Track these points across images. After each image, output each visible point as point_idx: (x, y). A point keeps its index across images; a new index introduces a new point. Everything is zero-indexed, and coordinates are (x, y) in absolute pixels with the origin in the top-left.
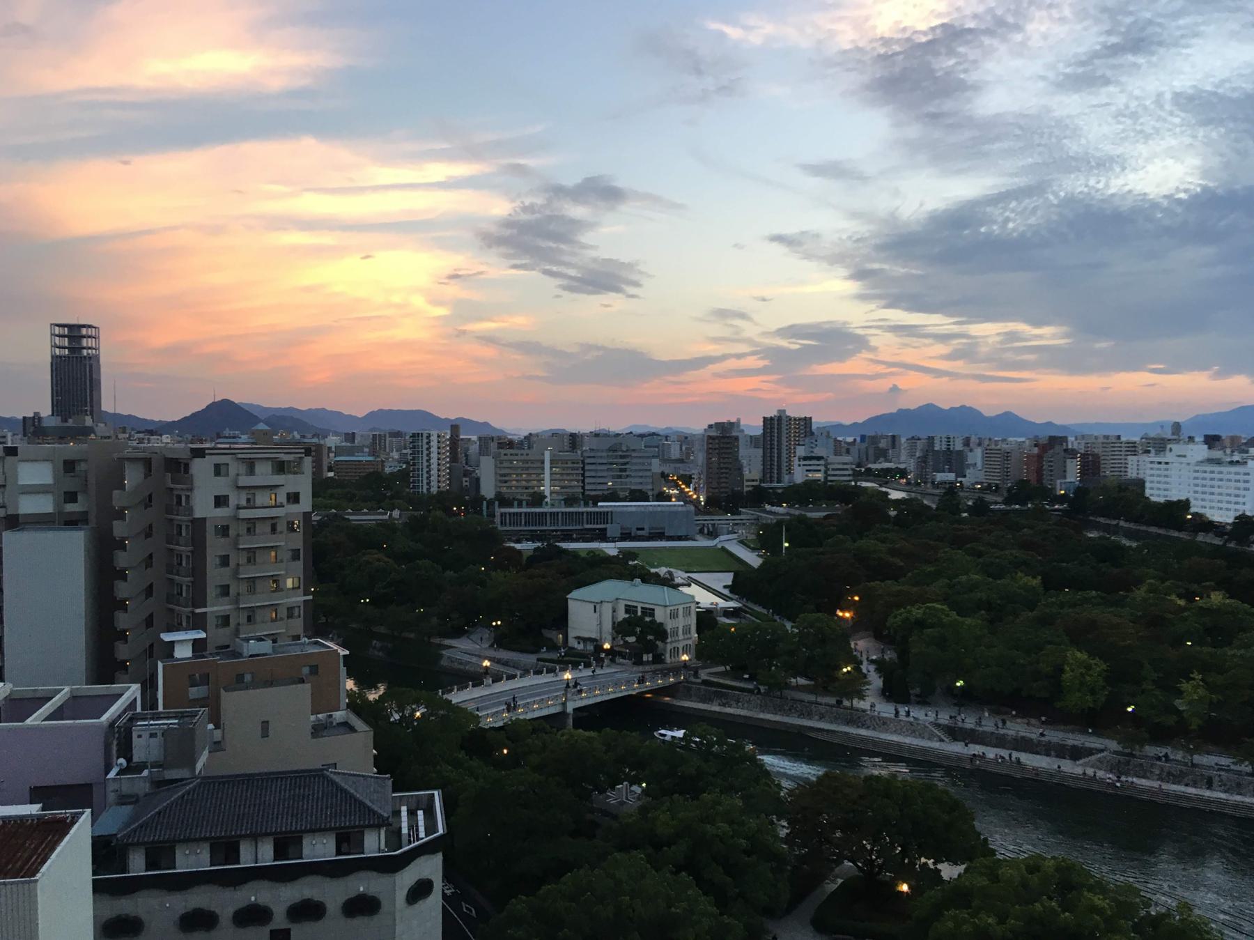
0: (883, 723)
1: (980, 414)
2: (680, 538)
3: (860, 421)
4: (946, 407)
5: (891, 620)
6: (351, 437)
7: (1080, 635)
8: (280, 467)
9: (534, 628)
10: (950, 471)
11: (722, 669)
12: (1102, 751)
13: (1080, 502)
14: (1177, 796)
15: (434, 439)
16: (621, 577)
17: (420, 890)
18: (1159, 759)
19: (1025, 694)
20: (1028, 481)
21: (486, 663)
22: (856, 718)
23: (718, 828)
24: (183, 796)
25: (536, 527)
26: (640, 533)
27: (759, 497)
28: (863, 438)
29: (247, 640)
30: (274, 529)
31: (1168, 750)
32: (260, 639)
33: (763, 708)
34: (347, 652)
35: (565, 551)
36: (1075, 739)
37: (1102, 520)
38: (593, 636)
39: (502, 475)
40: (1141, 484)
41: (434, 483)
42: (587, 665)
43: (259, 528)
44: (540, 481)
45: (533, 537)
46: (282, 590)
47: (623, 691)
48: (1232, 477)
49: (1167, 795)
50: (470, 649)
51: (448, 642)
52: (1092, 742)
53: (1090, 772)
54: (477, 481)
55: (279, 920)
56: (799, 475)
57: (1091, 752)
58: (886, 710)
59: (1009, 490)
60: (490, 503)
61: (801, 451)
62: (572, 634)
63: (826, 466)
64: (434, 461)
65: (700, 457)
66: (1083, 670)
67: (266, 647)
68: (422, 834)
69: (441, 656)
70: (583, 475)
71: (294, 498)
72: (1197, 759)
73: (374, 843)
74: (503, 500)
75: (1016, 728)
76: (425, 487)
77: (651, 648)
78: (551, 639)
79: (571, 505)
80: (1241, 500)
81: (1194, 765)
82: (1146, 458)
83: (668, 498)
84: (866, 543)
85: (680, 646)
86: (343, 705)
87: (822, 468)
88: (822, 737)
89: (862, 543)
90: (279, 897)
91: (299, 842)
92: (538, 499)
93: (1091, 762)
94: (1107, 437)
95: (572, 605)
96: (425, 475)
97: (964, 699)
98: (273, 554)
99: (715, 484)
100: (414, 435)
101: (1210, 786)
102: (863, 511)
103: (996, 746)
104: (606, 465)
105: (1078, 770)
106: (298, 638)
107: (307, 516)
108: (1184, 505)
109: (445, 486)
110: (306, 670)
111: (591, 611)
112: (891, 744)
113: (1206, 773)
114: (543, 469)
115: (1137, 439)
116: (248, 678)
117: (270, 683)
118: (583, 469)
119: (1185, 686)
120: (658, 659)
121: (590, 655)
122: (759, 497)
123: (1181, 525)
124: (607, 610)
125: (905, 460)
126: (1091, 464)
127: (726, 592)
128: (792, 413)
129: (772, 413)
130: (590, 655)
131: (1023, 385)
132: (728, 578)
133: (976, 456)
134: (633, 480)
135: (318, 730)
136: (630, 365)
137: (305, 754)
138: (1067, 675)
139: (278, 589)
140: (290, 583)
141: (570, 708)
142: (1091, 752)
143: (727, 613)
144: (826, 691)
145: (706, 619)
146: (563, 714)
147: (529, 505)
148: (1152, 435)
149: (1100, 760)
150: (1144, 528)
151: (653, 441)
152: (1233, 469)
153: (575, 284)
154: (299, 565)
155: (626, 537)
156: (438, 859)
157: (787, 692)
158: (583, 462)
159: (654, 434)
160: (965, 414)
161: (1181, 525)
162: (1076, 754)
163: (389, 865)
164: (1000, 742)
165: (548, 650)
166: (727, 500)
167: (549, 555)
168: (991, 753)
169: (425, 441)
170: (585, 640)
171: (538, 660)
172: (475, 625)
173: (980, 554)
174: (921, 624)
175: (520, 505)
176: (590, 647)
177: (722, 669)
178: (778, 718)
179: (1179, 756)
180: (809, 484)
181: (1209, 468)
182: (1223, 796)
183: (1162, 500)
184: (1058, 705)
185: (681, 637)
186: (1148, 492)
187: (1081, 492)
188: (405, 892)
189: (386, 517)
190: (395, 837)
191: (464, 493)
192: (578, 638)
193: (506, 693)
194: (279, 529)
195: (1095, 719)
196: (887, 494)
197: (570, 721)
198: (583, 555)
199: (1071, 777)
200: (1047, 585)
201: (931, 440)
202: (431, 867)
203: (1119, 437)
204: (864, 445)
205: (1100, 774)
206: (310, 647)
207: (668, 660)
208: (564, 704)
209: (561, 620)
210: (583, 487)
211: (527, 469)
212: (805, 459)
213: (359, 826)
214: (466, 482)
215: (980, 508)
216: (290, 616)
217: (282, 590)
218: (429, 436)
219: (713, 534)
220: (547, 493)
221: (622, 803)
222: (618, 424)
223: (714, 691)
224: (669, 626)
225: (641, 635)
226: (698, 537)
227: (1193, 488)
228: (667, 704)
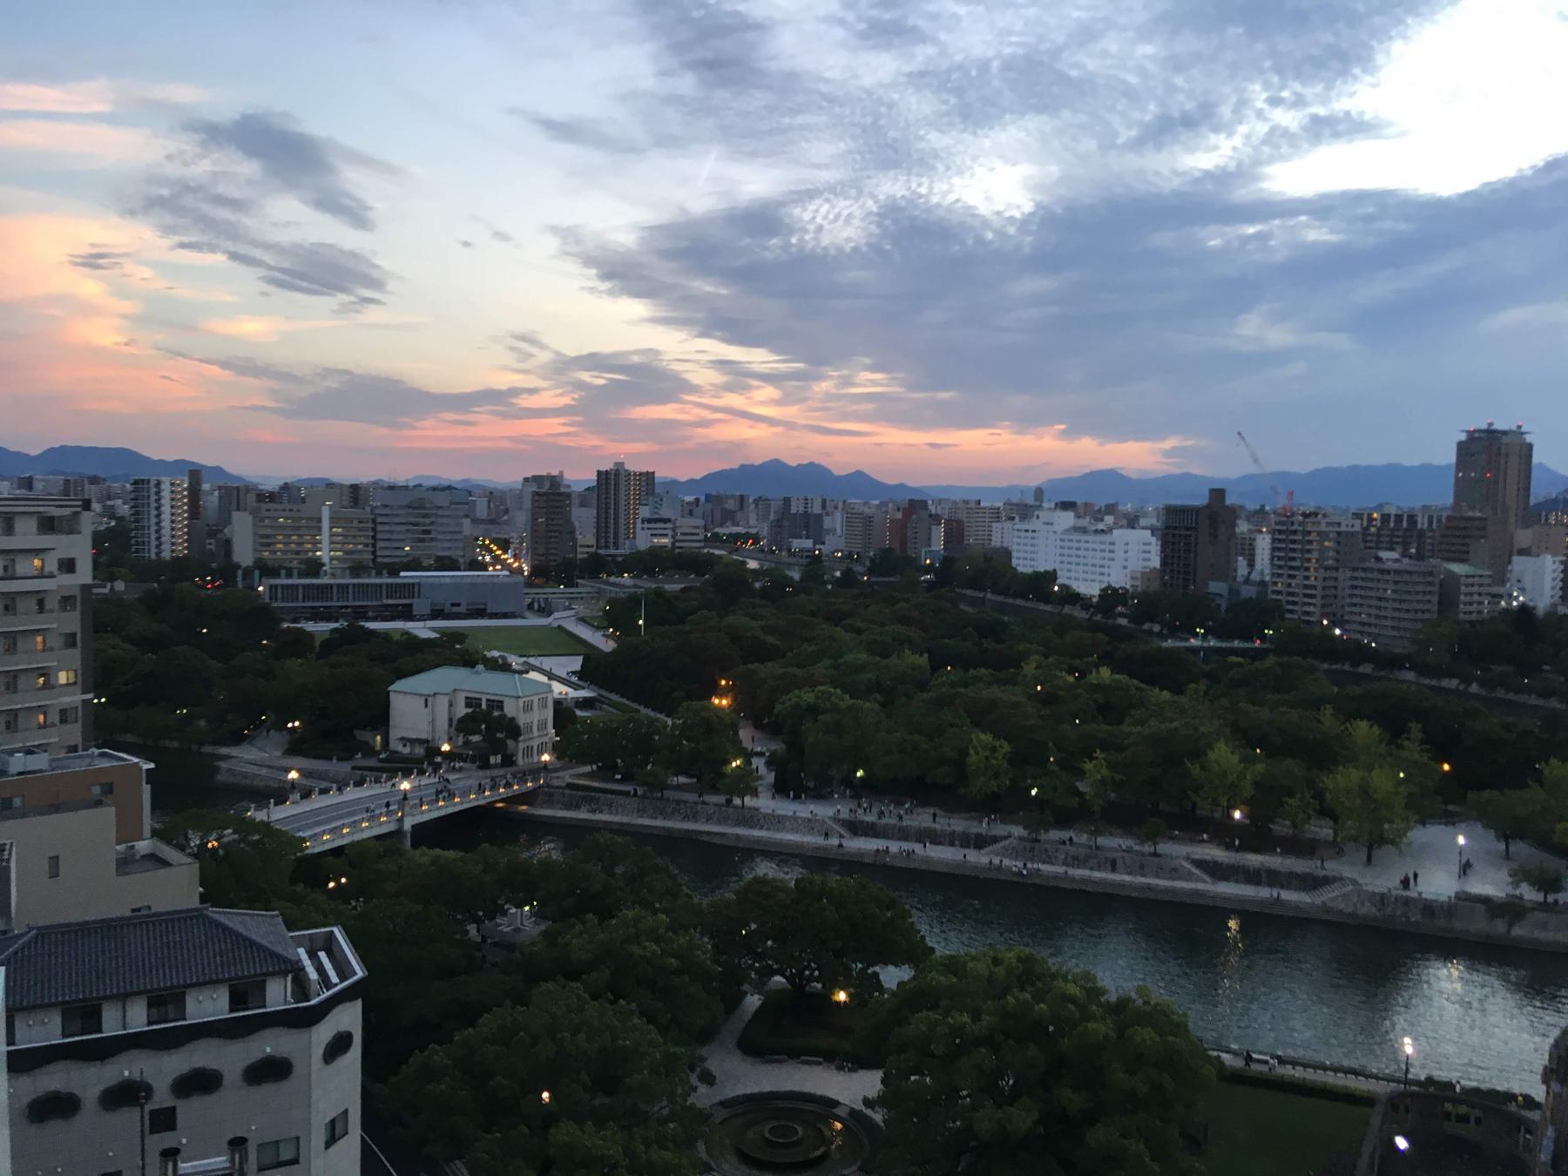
0: (777, 822)
1: (785, 465)
2: (505, 616)
3: (698, 477)
4: (794, 464)
5: (778, 707)
6: (28, 483)
7: (981, 716)
8: (48, 525)
9: (345, 726)
10: (808, 537)
11: (587, 769)
12: (1006, 838)
13: (947, 571)
14: (1084, 881)
15: (166, 487)
16: (452, 662)
17: (339, 1045)
18: (1064, 843)
19: (928, 784)
20: (890, 550)
21: (293, 775)
22: (750, 818)
23: (645, 948)
24: (16, 953)
25: (320, 602)
26: (455, 609)
27: (596, 566)
28: (708, 498)
29: (11, 753)
30: (41, 603)
31: (1071, 833)
32: (29, 751)
33: (641, 812)
34: (152, 766)
35: (373, 632)
36: (982, 828)
37: (968, 592)
38: (424, 736)
39: (262, 537)
40: (1007, 553)
41: (166, 547)
42: (421, 772)
43: (21, 605)
44: (316, 544)
45: (327, 616)
46: (53, 687)
47: (473, 800)
48: (1099, 547)
49: (1073, 879)
50: (250, 759)
51: (224, 751)
52: (999, 829)
53: (996, 861)
54: (228, 544)
55: (162, 1097)
56: (644, 540)
57: (995, 840)
58: (785, 807)
59: (872, 560)
60: (248, 573)
61: (645, 512)
62: (395, 734)
63: (674, 529)
64: (166, 517)
65: (521, 518)
66: (987, 753)
67: (40, 762)
68: (335, 979)
69: (218, 768)
70: (374, 537)
71: (68, 566)
72: (1101, 841)
73: (278, 996)
74: (266, 570)
75: (922, 819)
76: (153, 550)
77: (499, 747)
78: (366, 743)
79: (358, 576)
80: (1106, 570)
81: (1097, 848)
82: (1008, 525)
83: (483, 566)
84: (737, 619)
85: (535, 743)
86: (147, 832)
87: (670, 533)
88: (717, 841)
89: (731, 619)
90: (161, 1070)
91: (180, 1000)
92: (314, 568)
93: (1001, 851)
94: (966, 502)
95: (395, 700)
96: (153, 536)
97: (859, 791)
98: (39, 639)
99: (541, 550)
100: (136, 482)
101: (1114, 869)
102: (730, 586)
103: (900, 839)
104: (407, 522)
105: (985, 860)
106: (74, 749)
107: (85, 588)
108: (1051, 576)
109: (182, 550)
110: (97, 790)
111: (421, 706)
112: (788, 844)
113: (1111, 855)
114: (320, 529)
115: (1000, 504)
116: (17, 802)
117: (56, 808)
118: (374, 529)
119: (1089, 766)
120: (508, 761)
121: (424, 758)
122: (596, 566)
123: (1047, 597)
124: (442, 704)
125: (753, 523)
126: (955, 532)
127: (574, 679)
128: (634, 466)
129: (607, 466)
130: (424, 758)
131: (857, 440)
132: (576, 663)
133: (835, 522)
134: (439, 545)
135: (126, 864)
136: (390, 399)
137: (114, 897)
138: (973, 758)
139: (48, 686)
140: (63, 677)
141: (408, 825)
142: (995, 840)
143: (585, 704)
144: (715, 790)
145: (562, 713)
146: (398, 833)
147: (302, 575)
148: (1015, 501)
149: (1005, 848)
150: (1011, 601)
151: (457, 497)
152: (1099, 538)
153: (287, 278)
154: (75, 655)
155: (437, 614)
156: (357, 1006)
157: (667, 794)
158: (374, 521)
159: (449, 488)
160: (814, 473)
161: (1047, 597)
162: (980, 842)
163: (304, 1019)
164: (903, 834)
165: (364, 756)
166: (557, 569)
167: (352, 638)
168: (894, 847)
169: (154, 490)
170: (413, 742)
171: (354, 768)
172: (257, 728)
173: (859, 632)
174: (814, 710)
175: (289, 575)
176: (420, 751)
177: (587, 769)
178: (659, 823)
179: (1083, 838)
180: (655, 554)
181: (1075, 536)
182: (1127, 878)
183: (1029, 570)
184: (962, 791)
185: (536, 734)
186: (1014, 562)
187: (947, 561)
188: (321, 1051)
189: (106, 590)
190: (301, 988)
191: (209, 554)
192: (402, 739)
193: (333, 814)
194: (48, 605)
195: (998, 805)
196: (744, 563)
197: (408, 843)
198: (396, 637)
199: (976, 867)
200: (936, 666)
201: (787, 501)
202: (349, 1018)
203: (979, 502)
204: (709, 506)
205: (1006, 862)
206: (100, 761)
207: (520, 761)
208: (401, 820)
209: (381, 718)
210: (374, 552)
211: (299, 528)
212: (650, 521)
213: (179, 986)
214: (211, 545)
215: (849, 579)
216: (63, 721)
217: (53, 687)
218: (158, 484)
219: (545, 610)
220: (326, 560)
221: (517, 930)
222: (402, 473)
223: (578, 795)
224: (522, 720)
225: (488, 732)
226: (527, 614)
227: (1058, 558)
228: (524, 813)
